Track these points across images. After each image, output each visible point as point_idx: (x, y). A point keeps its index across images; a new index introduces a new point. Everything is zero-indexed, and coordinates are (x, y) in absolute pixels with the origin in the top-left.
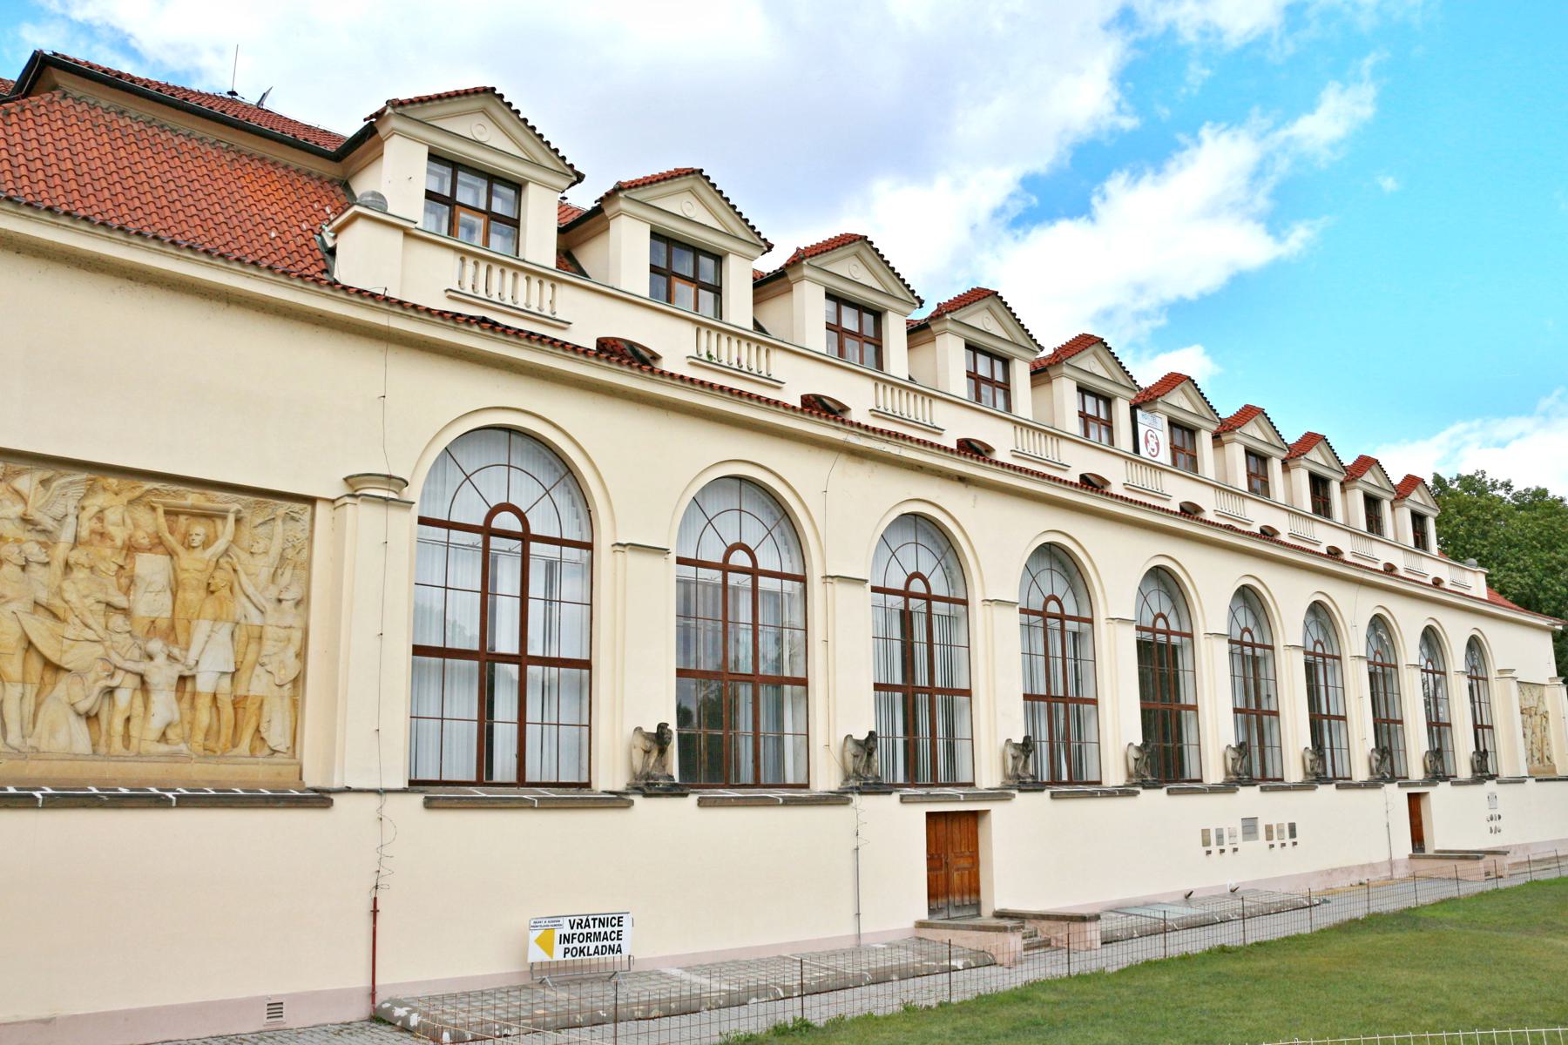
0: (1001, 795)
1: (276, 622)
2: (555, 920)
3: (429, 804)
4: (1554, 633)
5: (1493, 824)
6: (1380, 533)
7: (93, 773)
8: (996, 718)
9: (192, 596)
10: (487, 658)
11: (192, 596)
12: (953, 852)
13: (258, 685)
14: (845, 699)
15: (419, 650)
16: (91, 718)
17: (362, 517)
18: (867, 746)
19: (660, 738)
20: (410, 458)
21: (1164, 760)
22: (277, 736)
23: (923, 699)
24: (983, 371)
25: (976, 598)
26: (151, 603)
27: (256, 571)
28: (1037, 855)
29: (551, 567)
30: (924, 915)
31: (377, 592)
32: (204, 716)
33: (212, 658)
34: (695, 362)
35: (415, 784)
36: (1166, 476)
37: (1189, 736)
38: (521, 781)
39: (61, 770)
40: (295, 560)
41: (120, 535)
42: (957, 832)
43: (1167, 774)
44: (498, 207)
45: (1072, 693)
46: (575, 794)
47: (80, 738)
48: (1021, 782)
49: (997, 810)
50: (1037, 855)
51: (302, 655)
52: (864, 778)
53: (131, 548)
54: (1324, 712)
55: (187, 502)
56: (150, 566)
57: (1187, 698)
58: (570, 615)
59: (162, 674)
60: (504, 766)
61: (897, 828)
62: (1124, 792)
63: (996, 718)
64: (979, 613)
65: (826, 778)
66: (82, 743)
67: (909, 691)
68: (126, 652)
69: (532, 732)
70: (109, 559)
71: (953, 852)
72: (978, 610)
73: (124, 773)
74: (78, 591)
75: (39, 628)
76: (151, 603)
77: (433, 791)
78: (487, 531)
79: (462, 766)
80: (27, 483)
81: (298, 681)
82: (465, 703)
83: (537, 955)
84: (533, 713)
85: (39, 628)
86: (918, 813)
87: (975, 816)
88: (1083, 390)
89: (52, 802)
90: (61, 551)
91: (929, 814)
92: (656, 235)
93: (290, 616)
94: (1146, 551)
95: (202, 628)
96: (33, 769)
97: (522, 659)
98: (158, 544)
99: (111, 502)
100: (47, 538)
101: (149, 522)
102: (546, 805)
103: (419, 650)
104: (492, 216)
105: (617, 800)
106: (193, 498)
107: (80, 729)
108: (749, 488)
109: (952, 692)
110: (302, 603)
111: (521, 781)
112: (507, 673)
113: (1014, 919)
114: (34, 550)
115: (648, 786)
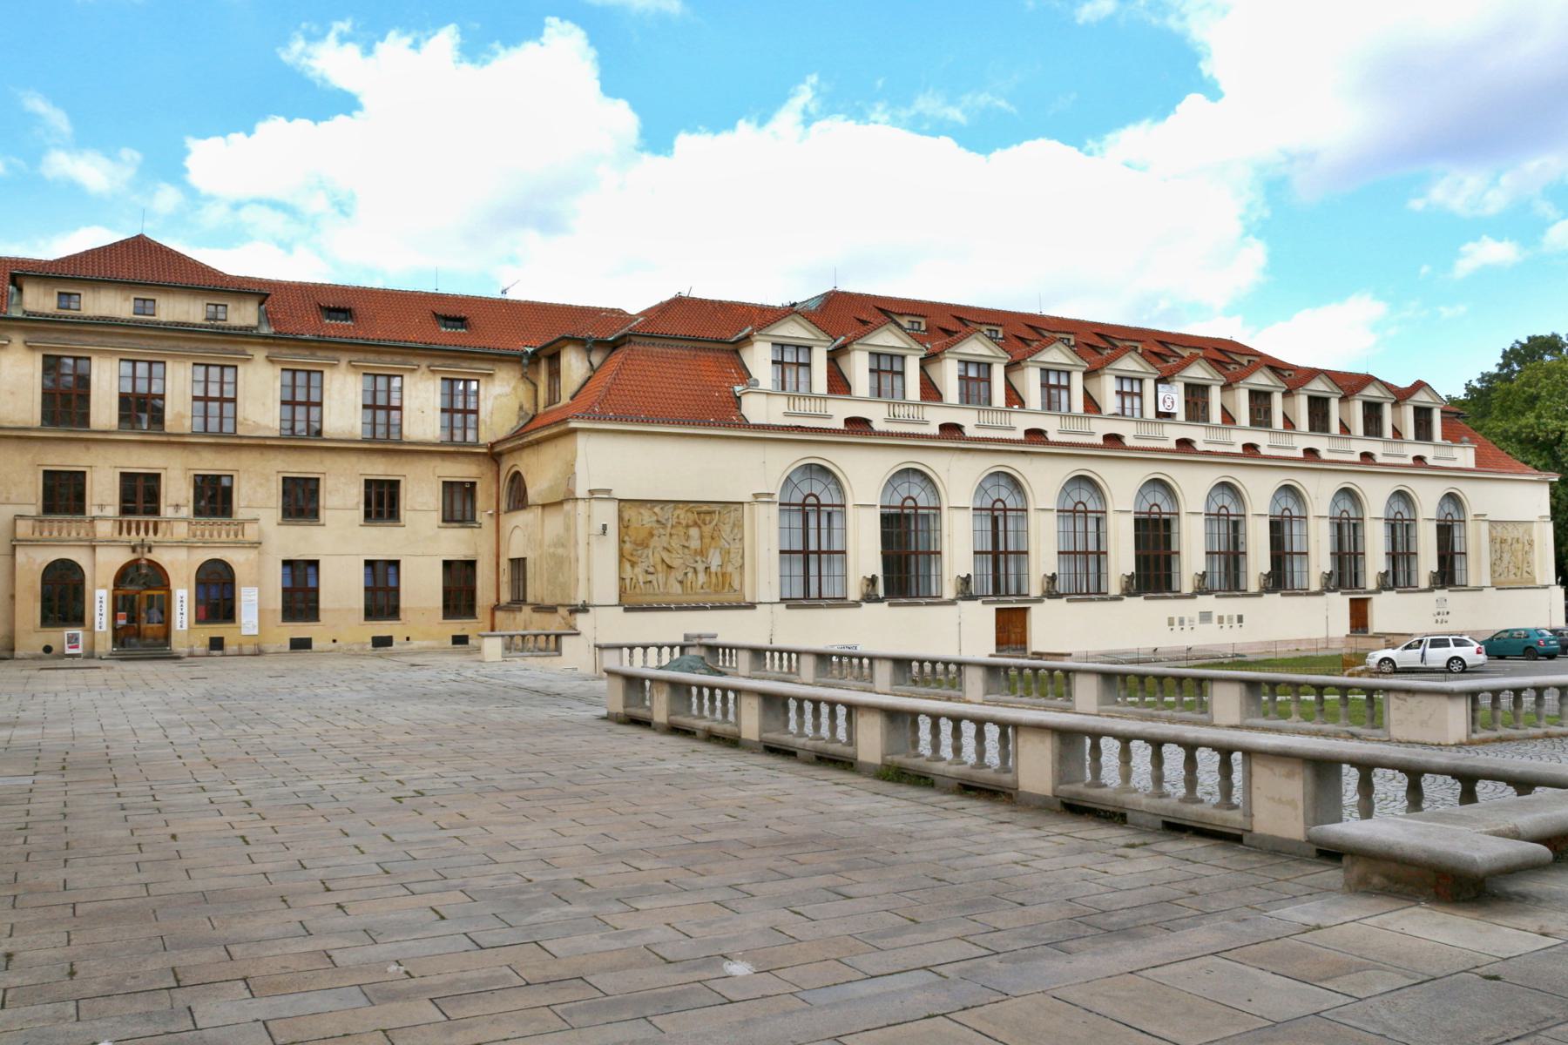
0: (1038, 600)
3: (788, 607)
4: (1551, 483)
5: (1176, 622)
6: (1022, 403)
7: (685, 599)
8: (1376, 561)
9: (707, 540)
10: (806, 553)
11: (707, 540)
12: (1359, 615)
13: (730, 569)
14: (1320, 560)
15: (782, 552)
18: (1053, 578)
20: (775, 487)
21: (1446, 576)
22: (736, 585)
23: (1002, 557)
24: (1127, 388)
25: (1031, 507)
28: (1388, 612)
29: (829, 514)
31: (766, 534)
32: (714, 579)
33: (715, 561)
34: (887, 421)
35: (782, 600)
36: (830, 402)
37: (1174, 568)
38: (820, 598)
39: (675, 599)
40: (738, 525)
43: (1443, 582)
44: (801, 360)
46: (841, 602)
47: (677, 588)
48: (1383, 587)
49: (1375, 597)
50: (1388, 612)
52: (966, 591)
53: (688, 526)
54: (1287, 549)
56: (694, 532)
57: (1174, 548)
58: (836, 533)
59: (700, 567)
60: (814, 592)
61: (1339, 604)
62: (1258, 595)
63: (1376, 561)
64: (1312, 522)
65: (1315, 586)
67: (996, 554)
68: (690, 562)
69: (824, 579)
70: (681, 530)
71: (1359, 615)
72: (1032, 514)
74: (675, 543)
75: (665, 555)
76: (695, 544)
77: (789, 602)
78: (804, 505)
79: (798, 592)
80: (657, 510)
81: (742, 566)
82: (798, 569)
84: (824, 572)
85: (665, 555)
86: (1346, 599)
87: (1025, 609)
88: (1121, 379)
92: (774, 344)
96: (668, 599)
97: (819, 552)
98: (696, 524)
99: (681, 512)
100: (664, 526)
101: (692, 517)
102: (829, 606)
103: (782, 552)
104: (799, 364)
105: (857, 604)
106: (705, 508)
108: (1226, 487)
109: (929, 553)
110: (742, 539)
111: (820, 598)
113: (1378, 636)
115: (870, 598)
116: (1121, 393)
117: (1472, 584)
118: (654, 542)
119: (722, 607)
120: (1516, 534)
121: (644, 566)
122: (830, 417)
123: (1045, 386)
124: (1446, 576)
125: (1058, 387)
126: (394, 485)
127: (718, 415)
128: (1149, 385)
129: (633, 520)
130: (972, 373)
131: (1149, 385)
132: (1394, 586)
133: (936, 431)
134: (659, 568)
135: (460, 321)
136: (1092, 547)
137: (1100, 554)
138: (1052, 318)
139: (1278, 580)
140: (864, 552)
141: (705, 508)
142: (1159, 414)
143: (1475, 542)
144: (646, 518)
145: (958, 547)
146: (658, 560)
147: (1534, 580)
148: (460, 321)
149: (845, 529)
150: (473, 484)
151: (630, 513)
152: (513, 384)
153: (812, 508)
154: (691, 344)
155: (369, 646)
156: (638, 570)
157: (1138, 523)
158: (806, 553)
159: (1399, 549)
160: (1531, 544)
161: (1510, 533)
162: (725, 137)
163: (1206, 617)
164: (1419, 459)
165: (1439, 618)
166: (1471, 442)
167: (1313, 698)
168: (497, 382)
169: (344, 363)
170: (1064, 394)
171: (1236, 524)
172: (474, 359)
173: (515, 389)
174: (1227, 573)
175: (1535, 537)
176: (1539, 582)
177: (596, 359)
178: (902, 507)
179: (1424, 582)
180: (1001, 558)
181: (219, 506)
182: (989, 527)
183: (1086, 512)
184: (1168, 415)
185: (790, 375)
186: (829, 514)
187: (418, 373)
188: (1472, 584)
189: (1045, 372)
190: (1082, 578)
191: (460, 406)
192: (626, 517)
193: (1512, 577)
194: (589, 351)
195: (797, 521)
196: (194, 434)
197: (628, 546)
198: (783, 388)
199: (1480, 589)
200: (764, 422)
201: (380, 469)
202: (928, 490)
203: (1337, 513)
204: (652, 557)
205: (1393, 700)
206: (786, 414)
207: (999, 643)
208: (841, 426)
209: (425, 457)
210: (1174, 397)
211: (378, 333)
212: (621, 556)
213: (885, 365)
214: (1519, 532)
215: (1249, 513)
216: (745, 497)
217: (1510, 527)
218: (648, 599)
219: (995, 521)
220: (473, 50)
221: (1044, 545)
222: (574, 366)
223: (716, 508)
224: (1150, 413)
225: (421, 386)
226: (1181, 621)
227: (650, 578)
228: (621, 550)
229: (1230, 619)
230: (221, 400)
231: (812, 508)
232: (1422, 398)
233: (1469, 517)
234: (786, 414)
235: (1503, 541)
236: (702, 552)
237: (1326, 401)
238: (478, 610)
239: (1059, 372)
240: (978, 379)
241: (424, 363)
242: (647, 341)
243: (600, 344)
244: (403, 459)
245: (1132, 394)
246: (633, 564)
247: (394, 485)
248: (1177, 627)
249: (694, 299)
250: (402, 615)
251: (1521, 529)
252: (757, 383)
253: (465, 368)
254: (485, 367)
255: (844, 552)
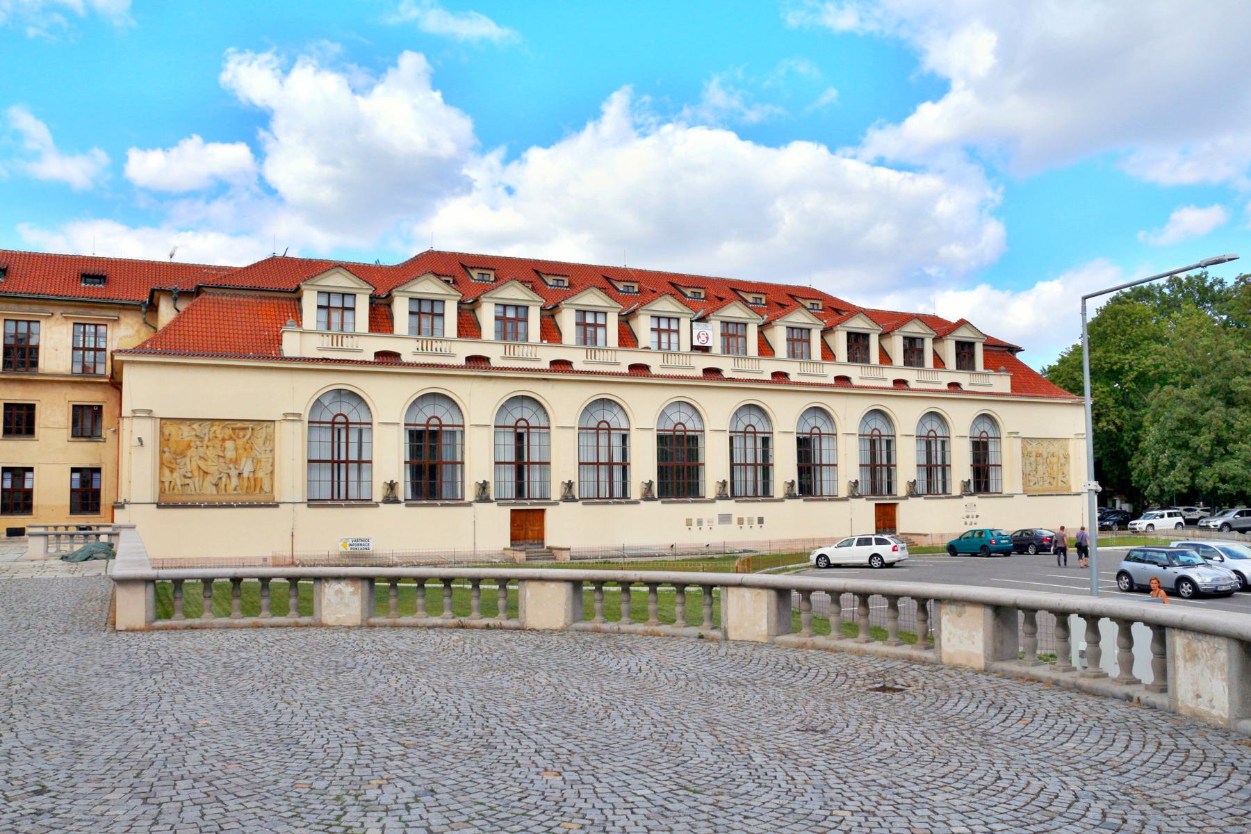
0: (906, 498)
1: (263, 457)
2: (347, 540)
5: (695, 522)
7: (217, 499)
9: (240, 451)
13: (260, 474)
16: (216, 485)
17: (287, 426)
19: (793, 483)
20: (303, 406)
21: (981, 481)
22: (266, 487)
26: (230, 454)
27: (259, 442)
29: (360, 431)
30: (508, 545)
33: (247, 469)
34: (415, 354)
36: (454, 344)
38: (347, 499)
39: (209, 498)
40: (270, 439)
41: (220, 437)
42: (888, 509)
45: (343, 458)
46: (366, 503)
48: (913, 492)
51: (273, 465)
52: (483, 495)
53: (224, 440)
55: (240, 428)
56: (229, 444)
57: (701, 461)
59: (234, 473)
65: (843, 492)
66: (214, 492)
68: (223, 467)
70: (218, 443)
72: (840, 437)
73: (225, 499)
74: (211, 453)
75: (202, 464)
76: (230, 454)
77: (313, 503)
78: (745, 432)
80: (195, 426)
81: (272, 472)
83: (342, 549)
85: (202, 464)
87: (543, 511)
89: (206, 507)
90: (206, 442)
91: (877, 505)
93: (269, 455)
94: (977, 409)
95: (244, 460)
96: (202, 498)
98: (231, 438)
103: (310, 461)
104: (344, 309)
106: (239, 425)
107: (214, 488)
111: (347, 499)
112: (343, 466)
114: (198, 443)
116: (659, 331)
117: (1006, 492)
118: (192, 452)
119: (251, 506)
120: (1051, 449)
121: (182, 471)
122: (618, 364)
123: (582, 324)
124: (981, 481)
125: (595, 325)
126: (31, 408)
127: (263, 351)
128: (685, 323)
129: (174, 433)
130: (511, 314)
131: (685, 323)
132: (930, 491)
133: (463, 362)
134: (196, 473)
135: (101, 278)
136: (617, 458)
137: (767, 468)
138: (635, 271)
139: (808, 483)
140: (389, 458)
141: (239, 425)
142: (694, 348)
143: (1008, 456)
144: (186, 433)
145: (480, 456)
146: (195, 467)
147: (1069, 488)
148: (101, 278)
149: (463, 444)
150: (100, 407)
151: (170, 429)
152: (136, 327)
153: (339, 428)
154: (258, 294)
155: (4, 536)
156: (175, 475)
157: (661, 439)
158: (335, 463)
159: (737, 460)
160: (1066, 457)
161: (1044, 449)
162: (739, 141)
163: (725, 519)
164: (954, 386)
165: (969, 521)
166: (1007, 371)
167: (470, 586)
168: (123, 326)
169: (58, 315)
170: (600, 332)
171: (766, 441)
172: (102, 308)
173: (138, 331)
174: (753, 480)
175: (1071, 452)
176: (1074, 490)
177: (183, 306)
178: (674, 431)
179: (956, 489)
180: (878, 473)
181: (23, 427)
182: (868, 447)
183: (755, 433)
184: (705, 349)
185: (336, 317)
186: (360, 431)
187: (54, 319)
188: (1006, 492)
189: (582, 313)
190: (607, 481)
191: (92, 346)
192: (167, 433)
193: (1047, 486)
194: (175, 299)
195: (326, 436)
196: (73, 374)
197: (167, 455)
198: (329, 328)
199: (1011, 496)
200: (298, 355)
201: (18, 395)
202: (764, 420)
203: (868, 431)
204: (190, 464)
205: (732, 591)
206: (319, 349)
207: (514, 538)
208: (371, 358)
209: (57, 385)
210: (711, 333)
211: (22, 288)
212: (162, 464)
213: (336, 302)
214: (1055, 448)
215: (953, 436)
216: (277, 416)
217: (1045, 444)
218: (184, 499)
219: (519, 437)
220: (318, 71)
221: (563, 457)
222: (166, 313)
223: (250, 425)
224: (686, 347)
225: (56, 329)
226: (700, 522)
227: (187, 481)
228: (161, 458)
229: (750, 521)
230: (96, 349)
231: (339, 428)
232: (964, 334)
233: (1004, 435)
234: (319, 349)
235: (1039, 455)
236: (236, 461)
237: (866, 336)
238: (102, 508)
239: (669, 319)
240: (516, 320)
241: (58, 312)
242: (219, 291)
243: (184, 294)
244: (38, 387)
245: (669, 331)
246: (172, 471)
247: (31, 408)
248: (695, 526)
249: (293, 260)
250: (34, 511)
251: (1056, 444)
252: (156, 318)
253: (95, 315)
254: (112, 314)
255: (370, 462)
